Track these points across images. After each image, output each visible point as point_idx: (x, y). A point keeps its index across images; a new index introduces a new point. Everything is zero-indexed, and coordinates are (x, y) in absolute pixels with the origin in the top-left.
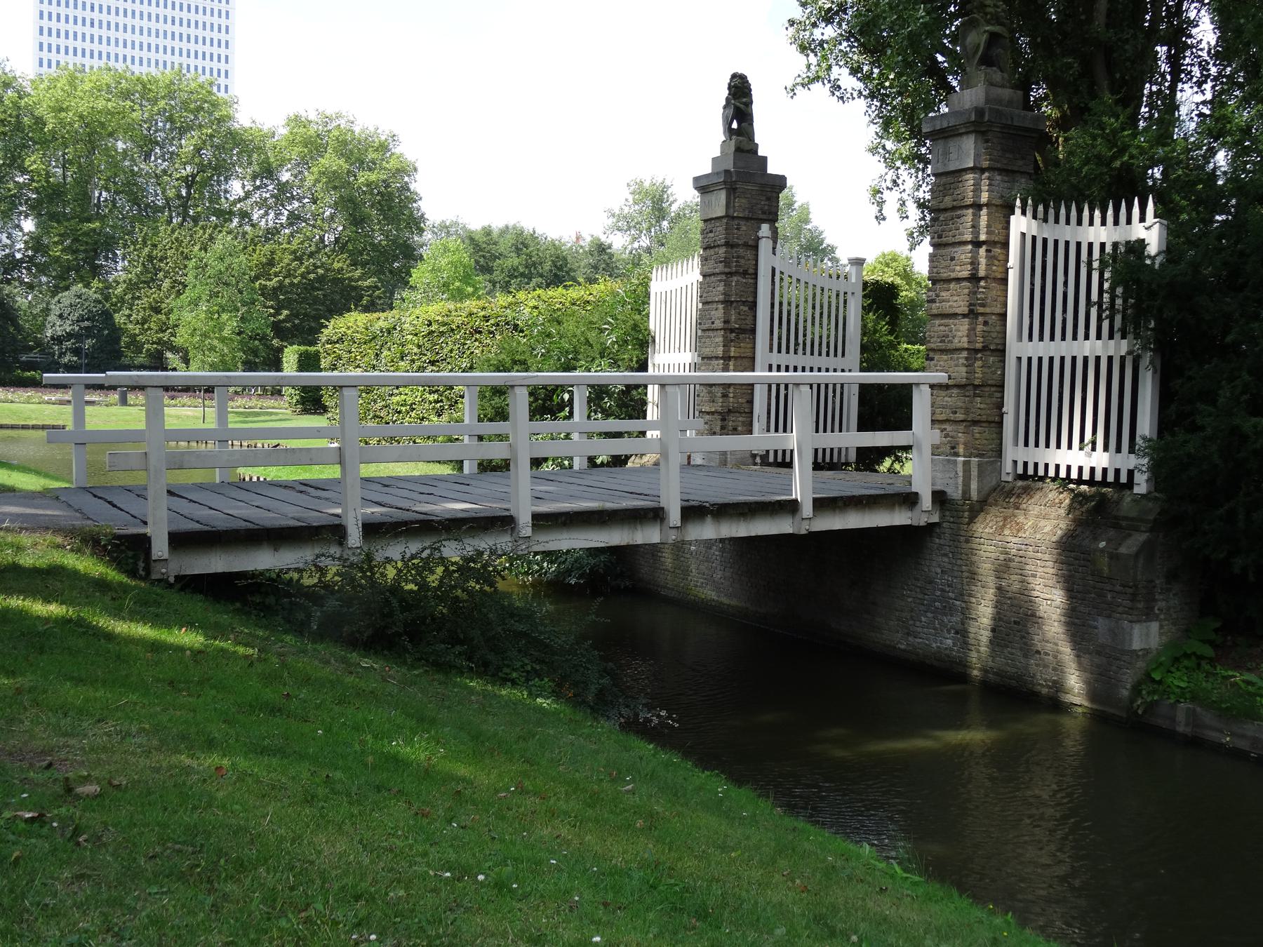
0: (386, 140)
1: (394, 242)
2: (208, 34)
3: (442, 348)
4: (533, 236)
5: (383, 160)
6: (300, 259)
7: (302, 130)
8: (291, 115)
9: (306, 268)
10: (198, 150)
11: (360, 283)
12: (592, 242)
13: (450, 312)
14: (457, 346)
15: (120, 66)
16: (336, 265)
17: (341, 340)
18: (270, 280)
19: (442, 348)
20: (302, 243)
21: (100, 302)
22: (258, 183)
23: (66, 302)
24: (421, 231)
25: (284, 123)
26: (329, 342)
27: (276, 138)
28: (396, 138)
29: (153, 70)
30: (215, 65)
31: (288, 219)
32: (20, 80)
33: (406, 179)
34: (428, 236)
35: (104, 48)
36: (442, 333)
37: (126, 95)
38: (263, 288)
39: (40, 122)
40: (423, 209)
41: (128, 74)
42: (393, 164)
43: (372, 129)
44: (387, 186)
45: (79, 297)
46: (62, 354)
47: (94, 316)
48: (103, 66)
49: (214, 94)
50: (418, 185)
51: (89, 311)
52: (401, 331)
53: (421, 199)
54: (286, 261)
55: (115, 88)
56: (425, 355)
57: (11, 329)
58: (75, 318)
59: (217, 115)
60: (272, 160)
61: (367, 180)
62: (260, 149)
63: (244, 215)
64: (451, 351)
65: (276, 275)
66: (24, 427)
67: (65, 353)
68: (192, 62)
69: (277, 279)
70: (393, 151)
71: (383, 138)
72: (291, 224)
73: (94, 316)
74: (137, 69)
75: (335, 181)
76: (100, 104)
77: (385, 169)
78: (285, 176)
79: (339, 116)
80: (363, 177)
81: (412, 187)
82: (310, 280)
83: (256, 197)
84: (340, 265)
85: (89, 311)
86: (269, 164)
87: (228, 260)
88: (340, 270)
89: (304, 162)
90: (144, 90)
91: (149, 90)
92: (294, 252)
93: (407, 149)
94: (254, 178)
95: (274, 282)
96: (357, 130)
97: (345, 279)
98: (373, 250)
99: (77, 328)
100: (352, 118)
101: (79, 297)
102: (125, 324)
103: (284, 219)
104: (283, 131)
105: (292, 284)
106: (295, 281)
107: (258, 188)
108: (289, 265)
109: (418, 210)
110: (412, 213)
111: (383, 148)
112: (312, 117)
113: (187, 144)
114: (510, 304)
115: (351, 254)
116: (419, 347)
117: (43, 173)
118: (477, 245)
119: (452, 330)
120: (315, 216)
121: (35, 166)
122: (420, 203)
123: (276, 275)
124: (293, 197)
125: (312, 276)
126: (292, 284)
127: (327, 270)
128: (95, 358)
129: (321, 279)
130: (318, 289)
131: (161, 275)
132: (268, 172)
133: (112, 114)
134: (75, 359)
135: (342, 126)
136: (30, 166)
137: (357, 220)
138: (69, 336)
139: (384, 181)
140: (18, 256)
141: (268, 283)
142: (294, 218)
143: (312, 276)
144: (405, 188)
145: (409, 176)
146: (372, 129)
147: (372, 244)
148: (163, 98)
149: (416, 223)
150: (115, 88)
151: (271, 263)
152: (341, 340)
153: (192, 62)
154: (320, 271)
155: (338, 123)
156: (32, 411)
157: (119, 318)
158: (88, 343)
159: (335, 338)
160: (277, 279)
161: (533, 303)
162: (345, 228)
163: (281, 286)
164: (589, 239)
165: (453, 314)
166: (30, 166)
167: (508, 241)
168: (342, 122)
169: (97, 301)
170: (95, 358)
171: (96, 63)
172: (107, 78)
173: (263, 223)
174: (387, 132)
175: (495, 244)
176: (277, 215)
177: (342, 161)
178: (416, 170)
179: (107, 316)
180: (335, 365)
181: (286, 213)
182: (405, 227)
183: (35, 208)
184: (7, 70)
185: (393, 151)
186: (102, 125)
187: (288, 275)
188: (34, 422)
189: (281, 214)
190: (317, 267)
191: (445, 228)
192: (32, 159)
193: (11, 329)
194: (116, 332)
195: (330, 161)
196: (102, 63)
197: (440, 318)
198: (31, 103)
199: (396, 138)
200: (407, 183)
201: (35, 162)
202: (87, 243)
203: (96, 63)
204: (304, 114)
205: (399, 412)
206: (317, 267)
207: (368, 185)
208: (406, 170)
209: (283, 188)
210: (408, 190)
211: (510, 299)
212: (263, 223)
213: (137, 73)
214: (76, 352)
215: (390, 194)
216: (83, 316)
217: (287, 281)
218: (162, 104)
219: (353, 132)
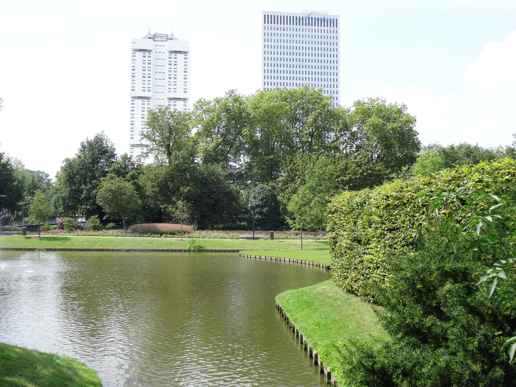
0: (401, 108)
1: (406, 155)
2: (329, 77)
3: (396, 219)
4: (476, 148)
5: (399, 117)
6: (360, 166)
7: (361, 107)
8: (356, 101)
9: (363, 170)
10: (315, 121)
11: (389, 176)
12: (507, 149)
13: (402, 188)
14: (408, 218)
15: (282, 87)
16: (377, 168)
17: (336, 211)
18: (346, 177)
19: (396, 219)
20: (361, 158)
21: (271, 191)
22: (343, 133)
23: (257, 191)
24: (419, 150)
25: (353, 105)
26: (330, 212)
27: (350, 112)
28: (405, 107)
29: (295, 87)
30: (332, 89)
31: (356, 148)
32: (242, 98)
33: (411, 125)
34: (422, 153)
35: (276, 81)
36: (397, 206)
37: (285, 99)
38: (343, 180)
39: (248, 114)
40: (420, 139)
41: (285, 91)
42: (404, 119)
43: (394, 104)
44: (402, 129)
45: (262, 189)
46: (255, 214)
47: (268, 197)
48: (276, 88)
49: (322, 95)
50: (417, 128)
51: (266, 195)
52: (369, 204)
53: (418, 134)
54: (353, 167)
55: (280, 97)
56: (385, 224)
57: (234, 204)
58: (260, 198)
59: (322, 103)
60: (348, 122)
61: (392, 127)
62: (343, 118)
63: (337, 149)
64: (403, 222)
65: (349, 174)
66: (225, 251)
67: (256, 214)
68: (310, 82)
69: (349, 176)
70: (404, 112)
71: (399, 107)
72: (357, 151)
73: (268, 197)
74: (288, 87)
75: (376, 128)
76: (272, 104)
77: (401, 121)
78: (355, 129)
79: (378, 99)
80: (390, 126)
81: (414, 129)
82: (364, 176)
83: (342, 139)
84: (379, 168)
85: (266, 195)
86: (346, 124)
87: (324, 168)
88: (379, 170)
89: (363, 122)
90: (292, 97)
91: (294, 96)
92: (357, 163)
93: (411, 111)
94: (340, 130)
95: (347, 178)
96: (387, 105)
97: (382, 175)
98: (396, 160)
99: (261, 203)
100: (384, 100)
101: (262, 189)
102: (282, 200)
103: (354, 149)
104: (353, 109)
105: (356, 178)
106: (357, 177)
107: (342, 135)
108: (354, 169)
109: (417, 139)
110: (414, 141)
111: (400, 112)
112: (366, 101)
113: (310, 119)
114: (454, 178)
115: (385, 162)
116: (381, 217)
117: (249, 136)
118: (447, 154)
119: (405, 204)
120: (369, 145)
121: (246, 133)
122: (418, 136)
123: (349, 174)
124: (357, 139)
125: (365, 174)
126: (356, 178)
127: (373, 171)
128: (268, 216)
129: (370, 175)
130: (369, 180)
131: (296, 178)
132: (346, 127)
133: (277, 108)
134: (260, 216)
135: (380, 104)
136: (243, 133)
137: (388, 147)
138: (258, 206)
139: (400, 127)
140: (243, 172)
141: (344, 178)
142: (358, 147)
143: (365, 174)
144: (411, 129)
145: (412, 124)
146: (394, 104)
147: (396, 157)
148: (300, 99)
149: (416, 146)
150: (280, 97)
151: (346, 169)
152: (336, 211)
153: (310, 82)
154: (370, 171)
155: (378, 102)
156: (230, 243)
157: (279, 198)
158: (265, 210)
159: (333, 210)
160: (349, 176)
161: (477, 176)
162: (382, 151)
163: (350, 179)
164: (505, 148)
165: (405, 189)
166: (243, 133)
167: (463, 151)
168: (380, 102)
169: (269, 190)
170: (268, 216)
171: (273, 87)
172: (277, 93)
173: (344, 152)
174: (401, 104)
175: (456, 153)
176: (352, 146)
177: (380, 120)
178: (415, 120)
179: (274, 197)
180: (334, 228)
181: (355, 146)
182: (411, 149)
183: (248, 152)
184: (236, 94)
185: (404, 112)
186: (274, 113)
187: (355, 174)
188: (230, 249)
189: (353, 146)
190: (368, 170)
191: (430, 147)
192: (245, 130)
193: (234, 204)
194: (278, 203)
195: (374, 120)
196: (275, 87)
197: (394, 194)
198: (245, 107)
199: (405, 107)
200: (411, 127)
201: (246, 131)
202: (268, 165)
203: (273, 87)
204: (362, 100)
205: (369, 268)
206: (368, 170)
207: (393, 129)
208: (411, 121)
209: (353, 134)
210: (412, 130)
211: (453, 173)
212: (344, 152)
213: (289, 90)
214: (261, 213)
215: (403, 133)
216: (263, 197)
217: (353, 177)
218: (299, 101)
219: (385, 106)
